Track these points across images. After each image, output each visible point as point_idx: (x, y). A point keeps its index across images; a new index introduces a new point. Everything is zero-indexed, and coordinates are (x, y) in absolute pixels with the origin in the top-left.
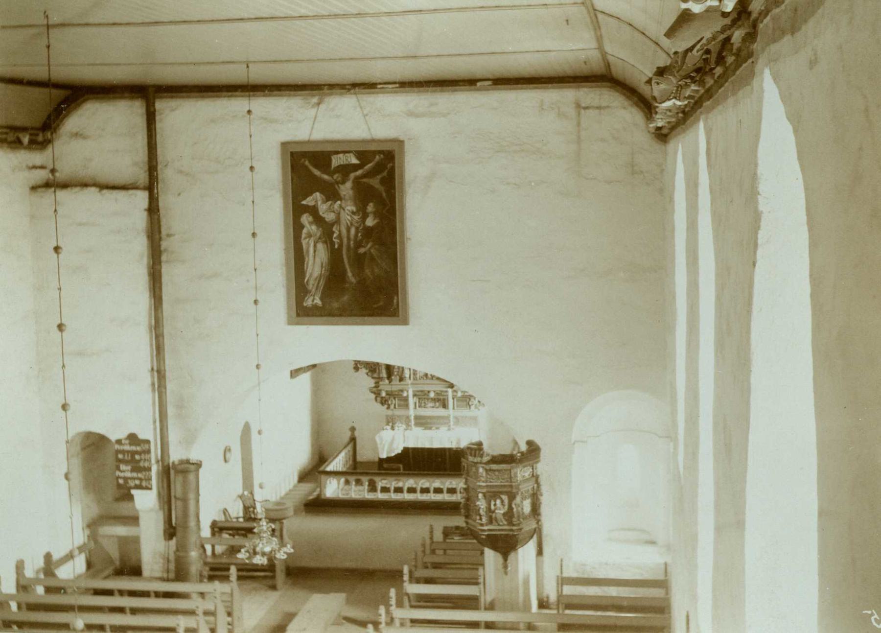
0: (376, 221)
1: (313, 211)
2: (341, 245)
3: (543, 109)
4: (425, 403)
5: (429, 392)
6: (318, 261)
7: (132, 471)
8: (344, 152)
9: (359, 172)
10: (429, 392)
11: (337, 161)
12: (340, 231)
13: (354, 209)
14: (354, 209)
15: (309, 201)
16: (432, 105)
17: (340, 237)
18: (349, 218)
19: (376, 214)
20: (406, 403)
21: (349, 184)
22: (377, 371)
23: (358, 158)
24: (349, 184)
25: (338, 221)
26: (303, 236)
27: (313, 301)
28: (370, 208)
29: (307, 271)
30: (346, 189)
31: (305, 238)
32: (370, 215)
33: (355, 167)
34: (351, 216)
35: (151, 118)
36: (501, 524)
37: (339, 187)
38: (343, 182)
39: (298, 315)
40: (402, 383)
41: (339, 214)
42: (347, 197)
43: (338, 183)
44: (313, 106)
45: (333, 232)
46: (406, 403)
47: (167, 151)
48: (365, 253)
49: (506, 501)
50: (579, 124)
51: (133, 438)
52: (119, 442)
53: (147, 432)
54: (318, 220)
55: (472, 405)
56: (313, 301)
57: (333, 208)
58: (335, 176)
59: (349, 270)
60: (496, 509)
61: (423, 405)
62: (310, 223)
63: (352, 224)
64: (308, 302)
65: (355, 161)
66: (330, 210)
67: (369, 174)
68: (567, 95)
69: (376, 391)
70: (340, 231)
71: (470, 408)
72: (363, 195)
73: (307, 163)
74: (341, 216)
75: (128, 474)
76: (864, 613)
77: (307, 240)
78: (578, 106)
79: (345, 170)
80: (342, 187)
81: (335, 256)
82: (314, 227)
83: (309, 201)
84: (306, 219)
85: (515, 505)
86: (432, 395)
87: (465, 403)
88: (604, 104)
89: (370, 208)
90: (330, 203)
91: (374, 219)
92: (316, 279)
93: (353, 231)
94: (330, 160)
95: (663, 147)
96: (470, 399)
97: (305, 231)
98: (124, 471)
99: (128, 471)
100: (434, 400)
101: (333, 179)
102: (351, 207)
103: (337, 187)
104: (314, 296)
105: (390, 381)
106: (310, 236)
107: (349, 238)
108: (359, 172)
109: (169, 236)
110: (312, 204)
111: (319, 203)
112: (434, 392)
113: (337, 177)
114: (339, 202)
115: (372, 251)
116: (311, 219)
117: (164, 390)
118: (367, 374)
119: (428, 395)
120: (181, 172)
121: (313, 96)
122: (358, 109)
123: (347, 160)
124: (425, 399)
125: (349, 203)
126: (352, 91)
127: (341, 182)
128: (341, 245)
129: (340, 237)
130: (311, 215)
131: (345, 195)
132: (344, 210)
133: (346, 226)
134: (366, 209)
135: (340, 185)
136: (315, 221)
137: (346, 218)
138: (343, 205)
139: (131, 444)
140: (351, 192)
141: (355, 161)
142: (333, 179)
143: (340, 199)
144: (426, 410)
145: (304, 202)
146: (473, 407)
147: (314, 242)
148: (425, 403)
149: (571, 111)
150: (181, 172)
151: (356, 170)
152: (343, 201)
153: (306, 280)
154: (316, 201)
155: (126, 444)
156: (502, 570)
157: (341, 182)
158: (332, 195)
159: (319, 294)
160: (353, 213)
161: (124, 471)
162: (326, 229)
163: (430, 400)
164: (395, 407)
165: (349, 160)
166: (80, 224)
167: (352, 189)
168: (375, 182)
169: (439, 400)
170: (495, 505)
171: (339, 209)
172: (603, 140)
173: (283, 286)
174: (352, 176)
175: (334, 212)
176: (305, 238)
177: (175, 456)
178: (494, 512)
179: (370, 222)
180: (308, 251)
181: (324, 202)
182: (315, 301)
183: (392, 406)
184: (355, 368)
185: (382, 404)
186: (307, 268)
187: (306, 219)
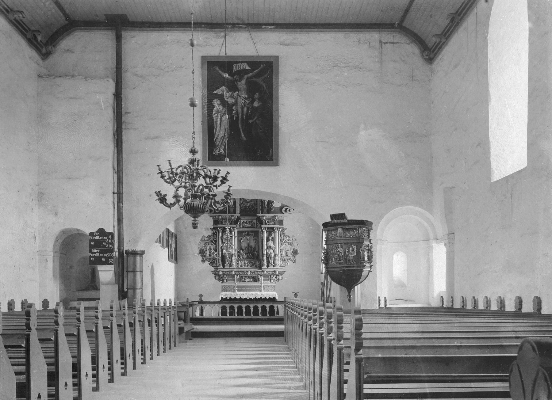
0: (260, 104)
1: (221, 97)
2: (237, 118)
3: (360, 43)
4: (244, 279)
5: (247, 272)
6: (223, 128)
7: (100, 253)
8: (241, 62)
9: (250, 74)
10: (247, 272)
11: (235, 68)
12: (237, 110)
13: (247, 96)
14: (247, 96)
15: (218, 92)
16: (295, 39)
17: (237, 113)
18: (243, 101)
19: (260, 99)
20: (233, 279)
21: (244, 82)
22: (216, 263)
23: (249, 66)
24: (244, 82)
25: (236, 104)
26: (214, 112)
27: (219, 151)
28: (256, 96)
29: (215, 133)
30: (242, 84)
31: (215, 114)
32: (256, 100)
33: (247, 72)
34: (244, 101)
35: (118, 39)
36: (352, 263)
37: (237, 83)
38: (240, 81)
39: (209, 159)
40: (231, 268)
41: (237, 99)
42: (242, 89)
43: (237, 81)
44: (222, 37)
45: (233, 110)
46: (233, 279)
47: (128, 62)
48: (253, 122)
49: (355, 250)
50: (382, 52)
51: (101, 231)
52: (92, 234)
53: (110, 227)
54: (223, 102)
55: (272, 279)
56: (219, 151)
57: (233, 95)
58: (235, 77)
59: (242, 134)
60: (349, 254)
61: (243, 280)
62: (219, 105)
63: (244, 105)
64: (216, 152)
65: (247, 68)
66: (233, 97)
67: (258, 75)
68: (375, 36)
69: (216, 274)
70: (237, 110)
71: (271, 281)
72: (252, 87)
73: (217, 69)
74: (238, 100)
75: (98, 255)
76: (508, 374)
77: (216, 115)
78: (381, 42)
79: (241, 73)
80: (239, 83)
81: (233, 124)
82: (221, 107)
83: (218, 92)
84: (216, 102)
85: (361, 250)
86: (249, 273)
87: (268, 278)
88: (395, 41)
89: (256, 96)
90: (231, 93)
91: (259, 103)
92: (221, 139)
93: (245, 109)
94: (233, 67)
95: (430, 66)
96: (271, 276)
97: (215, 109)
98: (95, 253)
99: (97, 252)
100: (249, 277)
101: (234, 78)
102: (244, 95)
103: (236, 83)
104: (220, 148)
105: (224, 266)
106: (218, 112)
107: (243, 114)
108: (250, 74)
109: (127, 113)
110: (220, 93)
111: (225, 93)
112: (250, 271)
113: (236, 77)
114: (237, 92)
115: (257, 121)
116: (219, 102)
117: (121, 205)
118: (210, 264)
119: (247, 274)
120: (136, 75)
121: (221, 32)
122: (250, 40)
123: (243, 67)
124: (244, 276)
125: (243, 93)
126: (246, 29)
127: (238, 80)
128: (237, 118)
129: (237, 113)
130: (219, 100)
131: (241, 88)
132: (240, 97)
133: (241, 106)
134: (254, 96)
135: (238, 82)
136: (221, 103)
137: (241, 102)
138: (240, 94)
139: (100, 236)
140: (245, 86)
141: (247, 68)
142: (234, 78)
143: (238, 91)
144: (245, 282)
145: (215, 92)
146: (272, 281)
147: (221, 116)
148: (244, 279)
149: (377, 45)
150: (136, 75)
151: (248, 73)
152: (240, 92)
153: (215, 139)
154: (223, 92)
155: (97, 235)
156: (347, 300)
157: (238, 80)
158: (233, 87)
159: (223, 147)
160: (245, 98)
161: (95, 253)
162: (229, 108)
163: (247, 277)
164: (227, 281)
165: (244, 67)
166: (71, 98)
167: (245, 84)
168: (260, 81)
169: (252, 277)
170: (349, 251)
171: (237, 97)
172: (395, 61)
173: (200, 144)
174: (246, 76)
175: (233, 98)
176: (215, 114)
177: (127, 247)
178: (347, 256)
179: (256, 104)
180: (217, 122)
181: (228, 92)
182: (220, 152)
183: (225, 281)
184: (202, 261)
185: (219, 280)
186: (216, 132)
187: (216, 102)
